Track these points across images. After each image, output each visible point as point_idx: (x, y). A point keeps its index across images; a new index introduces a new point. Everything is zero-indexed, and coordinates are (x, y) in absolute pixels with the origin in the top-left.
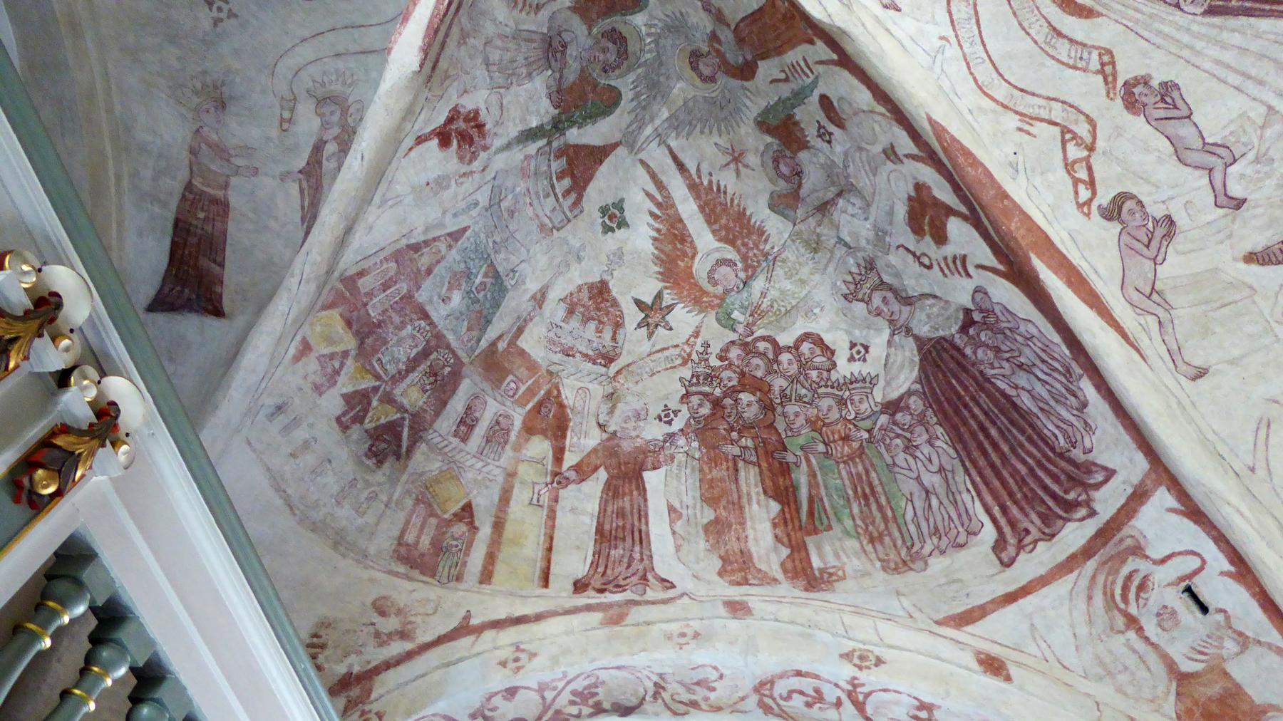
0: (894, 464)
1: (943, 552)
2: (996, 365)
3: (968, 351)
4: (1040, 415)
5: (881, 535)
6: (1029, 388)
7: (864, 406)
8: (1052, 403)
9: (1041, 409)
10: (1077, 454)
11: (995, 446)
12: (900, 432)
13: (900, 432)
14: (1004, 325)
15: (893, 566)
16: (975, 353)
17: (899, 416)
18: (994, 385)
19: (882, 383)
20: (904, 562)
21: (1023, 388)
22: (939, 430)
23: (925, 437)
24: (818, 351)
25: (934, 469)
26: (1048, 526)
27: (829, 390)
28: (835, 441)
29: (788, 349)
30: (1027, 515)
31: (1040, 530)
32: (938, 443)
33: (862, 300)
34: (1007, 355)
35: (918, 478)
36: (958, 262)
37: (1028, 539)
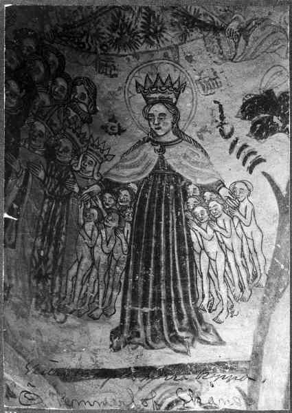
0: (83, 227)
1: (79, 316)
2: (204, 226)
3: (191, 201)
4: (205, 275)
5: (46, 277)
6: (213, 256)
7: (90, 168)
8: (221, 279)
9: (209, 275)
10: (208, 317)
11: (157, 268)
12: (101, 206)
13: (101, 206)
14: (237, 213)
15: (43, 306)
16: (195, 206)
17: (108, 195)
18: (189, 234)
19: (115, 161)
20: (53, 309)
21: (208, 254)
22: (128, 228)
23: (114, 224)
24: (86, 101)
25: (106, 250)
26: (153, 340)
27: (74, 136)
28: (53, 177)
29: (67, 78)
30: (145, 324)
31: (146, 339)
32: (121, 235)
33: (146, 99)
34: (216, 228)
35: (92, 248)
36: (252, 158)
37: (137, 340)
